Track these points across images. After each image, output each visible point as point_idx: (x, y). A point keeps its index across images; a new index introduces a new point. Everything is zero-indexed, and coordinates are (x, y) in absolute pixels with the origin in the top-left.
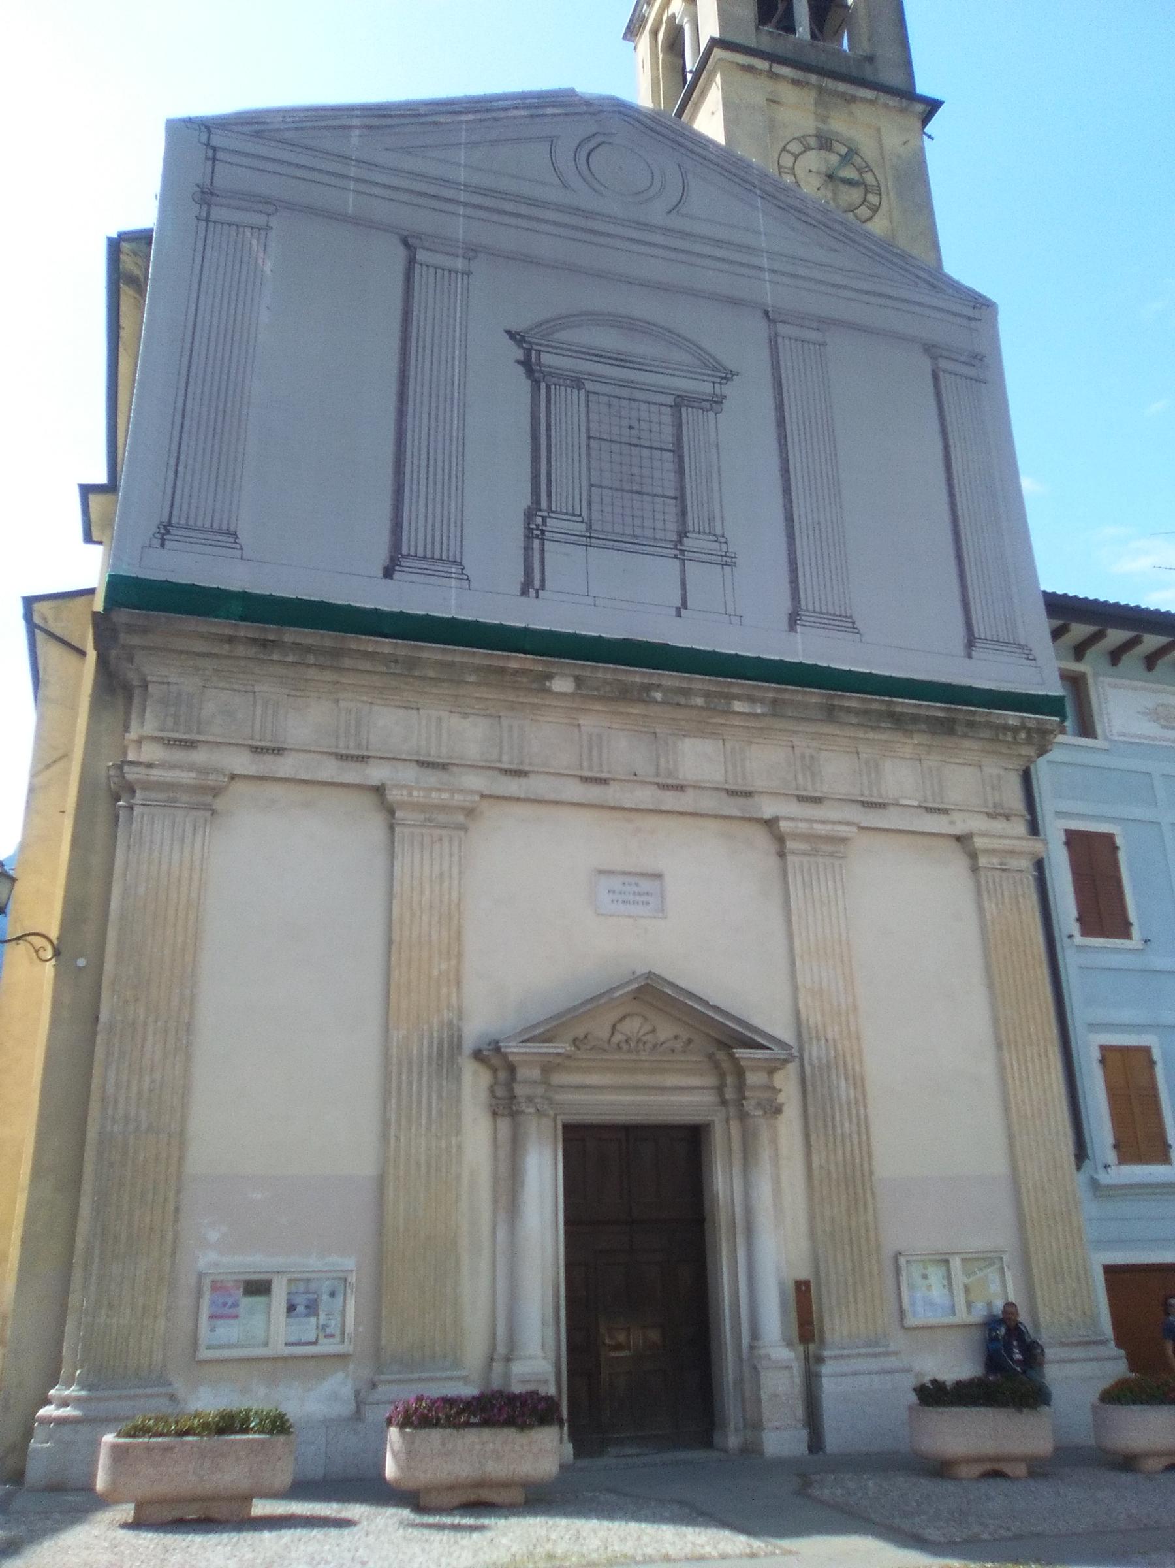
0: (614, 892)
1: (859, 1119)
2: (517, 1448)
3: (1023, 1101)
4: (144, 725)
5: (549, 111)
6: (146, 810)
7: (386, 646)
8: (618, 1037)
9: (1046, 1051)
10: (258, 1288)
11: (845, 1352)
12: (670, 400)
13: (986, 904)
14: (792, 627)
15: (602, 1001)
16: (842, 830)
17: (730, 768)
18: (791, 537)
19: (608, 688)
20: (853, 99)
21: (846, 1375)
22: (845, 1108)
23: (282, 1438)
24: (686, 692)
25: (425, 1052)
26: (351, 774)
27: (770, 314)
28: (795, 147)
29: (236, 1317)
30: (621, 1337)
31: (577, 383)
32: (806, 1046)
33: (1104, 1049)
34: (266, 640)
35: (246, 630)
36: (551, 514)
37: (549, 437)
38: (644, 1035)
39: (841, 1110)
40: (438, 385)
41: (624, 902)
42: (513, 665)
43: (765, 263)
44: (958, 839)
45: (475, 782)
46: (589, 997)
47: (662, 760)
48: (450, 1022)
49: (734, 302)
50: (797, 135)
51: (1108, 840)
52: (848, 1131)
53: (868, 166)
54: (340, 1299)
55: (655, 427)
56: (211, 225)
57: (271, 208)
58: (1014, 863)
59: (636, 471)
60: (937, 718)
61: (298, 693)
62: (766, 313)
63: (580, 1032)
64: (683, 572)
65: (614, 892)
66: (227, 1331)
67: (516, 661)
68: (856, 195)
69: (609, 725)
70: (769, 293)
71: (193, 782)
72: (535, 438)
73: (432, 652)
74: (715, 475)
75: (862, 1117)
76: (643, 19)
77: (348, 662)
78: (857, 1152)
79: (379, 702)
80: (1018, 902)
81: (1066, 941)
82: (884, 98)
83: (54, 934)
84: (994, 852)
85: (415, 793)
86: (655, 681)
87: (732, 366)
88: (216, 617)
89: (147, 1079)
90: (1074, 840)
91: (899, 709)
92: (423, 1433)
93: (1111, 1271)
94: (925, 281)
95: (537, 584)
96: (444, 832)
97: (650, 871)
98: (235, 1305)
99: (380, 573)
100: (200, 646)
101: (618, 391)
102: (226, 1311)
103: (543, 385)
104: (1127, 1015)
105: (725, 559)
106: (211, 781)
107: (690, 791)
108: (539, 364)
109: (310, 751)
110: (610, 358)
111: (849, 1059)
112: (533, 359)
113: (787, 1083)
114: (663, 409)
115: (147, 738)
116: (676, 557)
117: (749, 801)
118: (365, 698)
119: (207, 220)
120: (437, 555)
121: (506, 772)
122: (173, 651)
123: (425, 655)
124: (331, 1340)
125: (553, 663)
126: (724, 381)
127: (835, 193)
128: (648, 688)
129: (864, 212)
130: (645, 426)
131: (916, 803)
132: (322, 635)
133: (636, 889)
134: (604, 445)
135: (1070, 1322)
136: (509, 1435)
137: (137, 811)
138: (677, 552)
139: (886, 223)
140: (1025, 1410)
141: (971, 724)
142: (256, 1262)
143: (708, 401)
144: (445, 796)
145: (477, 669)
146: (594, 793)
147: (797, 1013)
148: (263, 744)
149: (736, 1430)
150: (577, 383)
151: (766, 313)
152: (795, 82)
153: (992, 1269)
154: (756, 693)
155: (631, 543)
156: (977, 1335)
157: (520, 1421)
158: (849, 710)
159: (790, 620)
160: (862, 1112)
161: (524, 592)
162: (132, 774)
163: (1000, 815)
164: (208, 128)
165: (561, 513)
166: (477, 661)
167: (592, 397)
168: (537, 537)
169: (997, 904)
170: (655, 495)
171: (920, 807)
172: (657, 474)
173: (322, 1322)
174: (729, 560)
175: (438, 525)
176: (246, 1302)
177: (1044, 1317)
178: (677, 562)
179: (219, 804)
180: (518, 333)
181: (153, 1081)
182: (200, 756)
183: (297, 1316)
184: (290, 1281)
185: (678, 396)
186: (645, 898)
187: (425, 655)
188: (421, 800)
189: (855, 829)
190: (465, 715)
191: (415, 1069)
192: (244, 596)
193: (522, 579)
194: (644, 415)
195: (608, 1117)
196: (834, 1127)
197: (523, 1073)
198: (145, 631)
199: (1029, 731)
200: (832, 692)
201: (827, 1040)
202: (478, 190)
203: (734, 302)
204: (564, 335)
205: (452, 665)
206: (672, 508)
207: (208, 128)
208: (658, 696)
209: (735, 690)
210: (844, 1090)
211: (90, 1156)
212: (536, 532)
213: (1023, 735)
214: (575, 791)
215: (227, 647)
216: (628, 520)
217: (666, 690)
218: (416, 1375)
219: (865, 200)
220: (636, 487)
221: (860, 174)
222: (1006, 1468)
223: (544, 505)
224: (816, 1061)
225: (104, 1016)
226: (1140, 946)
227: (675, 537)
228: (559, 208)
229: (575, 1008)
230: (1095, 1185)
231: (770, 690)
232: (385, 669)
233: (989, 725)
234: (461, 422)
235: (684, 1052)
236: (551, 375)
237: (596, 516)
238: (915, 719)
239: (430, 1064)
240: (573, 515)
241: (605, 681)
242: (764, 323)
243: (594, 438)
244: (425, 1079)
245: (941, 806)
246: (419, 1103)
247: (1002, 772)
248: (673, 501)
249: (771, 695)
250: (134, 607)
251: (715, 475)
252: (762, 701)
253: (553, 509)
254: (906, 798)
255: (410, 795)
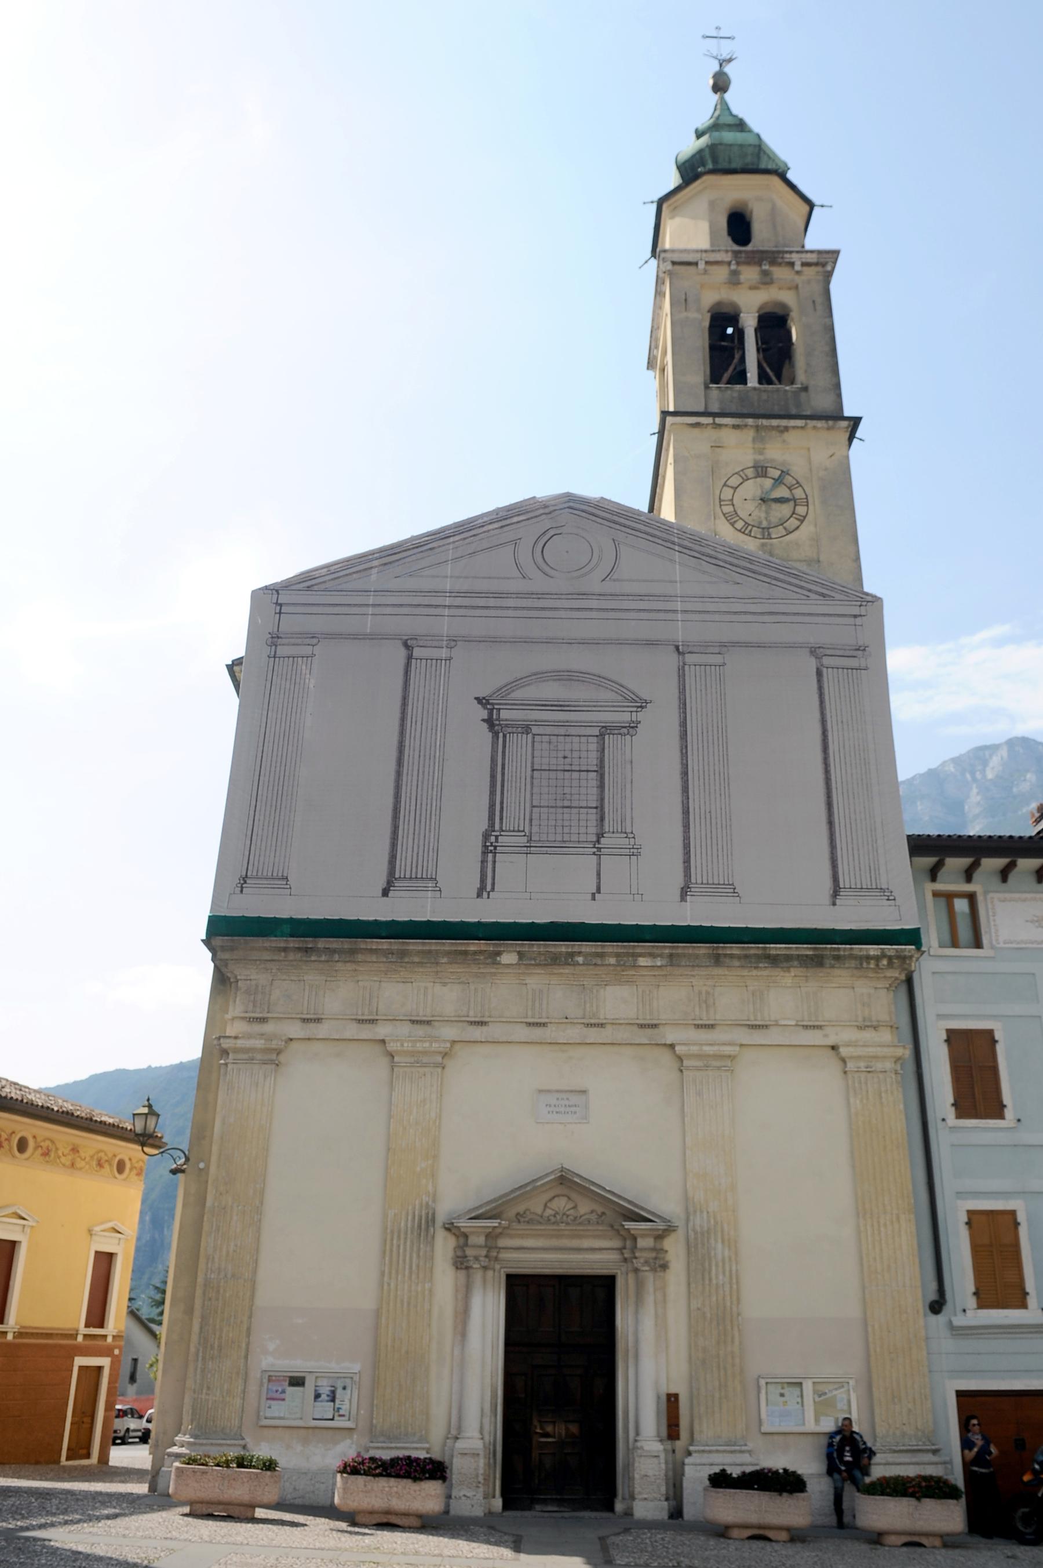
0: (550, 1106)
1: (731, 1271)
2: (412, 1492)
3: (875, 1259)
4: (236, 1008)
5: (515, 519)
6: (235, 1066)
7: (384, 944)
8: (549, 1212)
9: (898, 1219)
10: (297, 1382)
11: (707, 1448)
12: (596, 731)
13: (852, 1100)
14: (683, 897)
15: (528, 1188)
16: (727, 1050)
17: (641, 1006)
18: (686, 827)
19: (543, 958)
20: (787, 429)
21: (704, 1465)
22: (720, 1264)
23: (269, 1473)
24: (602, 955)
25: (409, 1225)
26: (366, 1032)
27: (680, 647)
28: (734, 481)
29: (283, 1400)
30: (549, 1429)
31: (527, 729)
32: (691, 1218)
33: (970, 1213)
34: (307, 948)
35: (293, 943)
36: (502, 833)
37: (503, 774)
38: (569, 1210)
39: (717, 1265)
40: (425, 748)
41: (557, 1112)
42: (472, 948)
43: (679, 606)
44: (833, 1048)
45: (449, 1032)
46: (516, 1187)
47: (588, 1005)
48: (427, 1204)
49: (651, 643)
50: (737, 470)
51: (988, 1038)
52: (721, 1282)
53: (798, 483)
54: (348, 1391)
55: (584, 754)
56: (277, 659)
57: (315, 641)
58: (879, 1066)
59: (567, 790)
60: (807, 956)
61: (333, 979)
62: (677, 648)
63: (521, 1208)
64: (599, 864)
65: (550, 1106)
66: (277, 1409)
67: (473, 946)
68: (786, 509)
69: (548, 982)
70: (680, 633)
71: (263, 1047)
72: (493, 777)
73: (415, 945)
74: (628, 786)
75: (734, 1272)
76: (655, 358)
77: (360, 957)
78: (728, 1298)
79: (385, 980)
80: (881, 1098)
81: (940, 1124)
82: (811, 423)
83: (185, 1147)
84: (859, 1058)
85: (406, 1045)
86: (576, 949)
87: (645, 696)
88: (276, 936)
89: (232, 1244)
90: (953, 1037)
91: (773, 952)
92: (353, 1477)
93: (960, 1394)
94: (816, 593)
95: (489, 888)
96: (426, 1070)
97: (578, 1089)
98: (283, 1392)
99: (380, 893)
100: (266, 956)
101: (556, 731)
102: (277, 1395)
103: (501, 735)
104: (995, 1185)
105: (632, 850)
106: (274, 1044)
107: (608, 1027)
108: (498, 719)
109: (338, 1019)
110: (552, 706)
111: (725, 1226)
112: (494, 717)
113: (674, 1248)
114: (591, 739)
115: (237, 1017)
116: (594, 854)
117: (656, 1031)
118: (375, 979)
119: (275, 657)
120: (419, 876)
121: (472, 1023)
122: (250, 960)
123: (411, 947)
124: (343, 1418)
125: (500, 945)
126: (639, 709)
127: (767, 513)
128: (572, 955)
129: (793, 523)
130: (576, 754)
131: (793, 1023)
132: (342, 942)
133: (567, 1102)
134: (545, 774)
135: (904, 1434)
136: (407, 1483)
137: (230, 1066)
138: (595, 850)
139: (812, 528)
140: (785, 1494)
141: (837, 958)
142: (297, 1365)
143: (625, 727)
144: (427, 1045)
145: (448, 953)
146: (537, 1033)
147: (686, 1192)
148: (308, 1016)
149: (624, 1499)
150: (527, 729)
151: (677, 648)
152: (735, 427)
153: (842, 1390)
154: (658, 951)
155: (561, 847)
156: (824, 1441)
157: (412, 1476)
158: (732, 956)
159: (682, 892)
160: (734, 1268)
161: (479, 895)
162: (226, 1044)
163: (868, 1026)
164: (277, 591)
165: (510, 831)
166: (447, 948)
167: (537, 738)
168: (491, 852)
169: (861, 1101)
170: (581, 807)
171: (797, 1025)
172: (583, 791)
173: (337, 1406)
174: (635, 851)
175: (421, 853)
176: (291, 1390)
177: (880, 1430)
178: (595, 857)
179: (282, 1058)
180: (484, 698)
181: (236, 1246)
182: (268, 1028)
183: (321, 1401)
184: (317, 1378)
185: (603, 727)
186: (573, 1109)
187: (411, 947)
188: (410, 1049)
189: (737, 1048)
190: (445, 984)
191: (402, 1236)
192: (291, 921)
193: (479, 886)
194: (576, 746)
195: (539, 1270)
196: (710, 1280)
197: (473, 1240)
198: (232, 949)
199: (890, 958)
200: (715, 945)
201: (708, 1212)
202: (459, 594)
203: (651, 643)
204: (518, 694)
205: (430, 952)
206: (593, 816)
207: (277, 591)
208: (580, 959)
209: (638, 950)
210: (720, 1250)
211: (199, 1292)
212: (490, 848)
213: (885, 962)
214: (523, 1033)
215: (283, 954)
216: (559, 830)
217: (586, 956)
218: (393, 1445)
219: (794, 513)
220: (567, 803)
221: (791, 491)
222: (770, 1534)
223: (497, 827)
224: (698, 1229)
225: (209, 1203)
226: (1012, 1125)
227: (594, 839)
228: (519, 595)
229: (506, 1195)
230: (951, 1326)
231: (666, 948)
232: (385, 960)
233: (852, 957)
234: (440, 772)
235: (598, 1223)
236: (507, 726)
237: (535, 829)
238: (788, 958)
239: (412, 1233)
240: (519, 831)
241: (540, 953)
242: (675, 655)
243: (537, 770)
244: (408, 1243)
245: (816, 1023)
246: (404, 1261)
247: (872, 991)
248: (595, 810)
249: (667, 951)
250: (224, 936)
251: (628, 786)
252: (661, 956)
253: (504, 829)
254: (785, 1019)
255: (402, 1045)
